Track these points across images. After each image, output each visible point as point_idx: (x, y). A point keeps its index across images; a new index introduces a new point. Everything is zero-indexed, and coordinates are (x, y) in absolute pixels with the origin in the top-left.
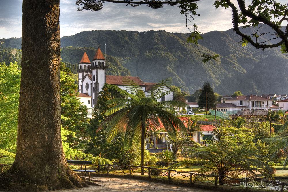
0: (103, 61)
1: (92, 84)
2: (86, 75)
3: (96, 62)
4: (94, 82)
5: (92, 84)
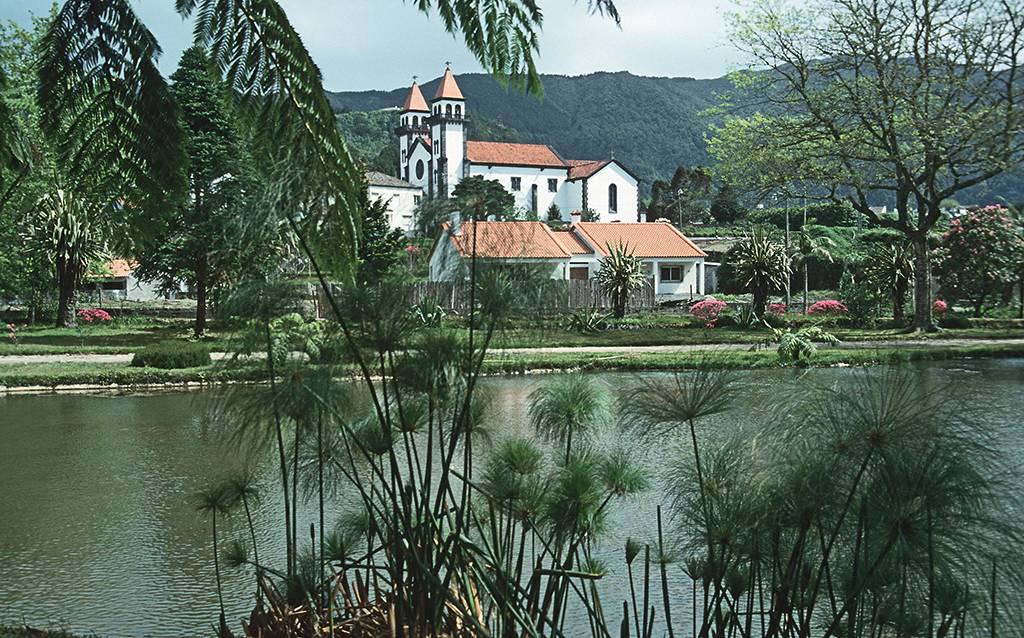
0: (459, 103)
1: (430, 162)
2: (417, 141)
3: (440, 106)
4: (437, 156)
5: (430, 162)
